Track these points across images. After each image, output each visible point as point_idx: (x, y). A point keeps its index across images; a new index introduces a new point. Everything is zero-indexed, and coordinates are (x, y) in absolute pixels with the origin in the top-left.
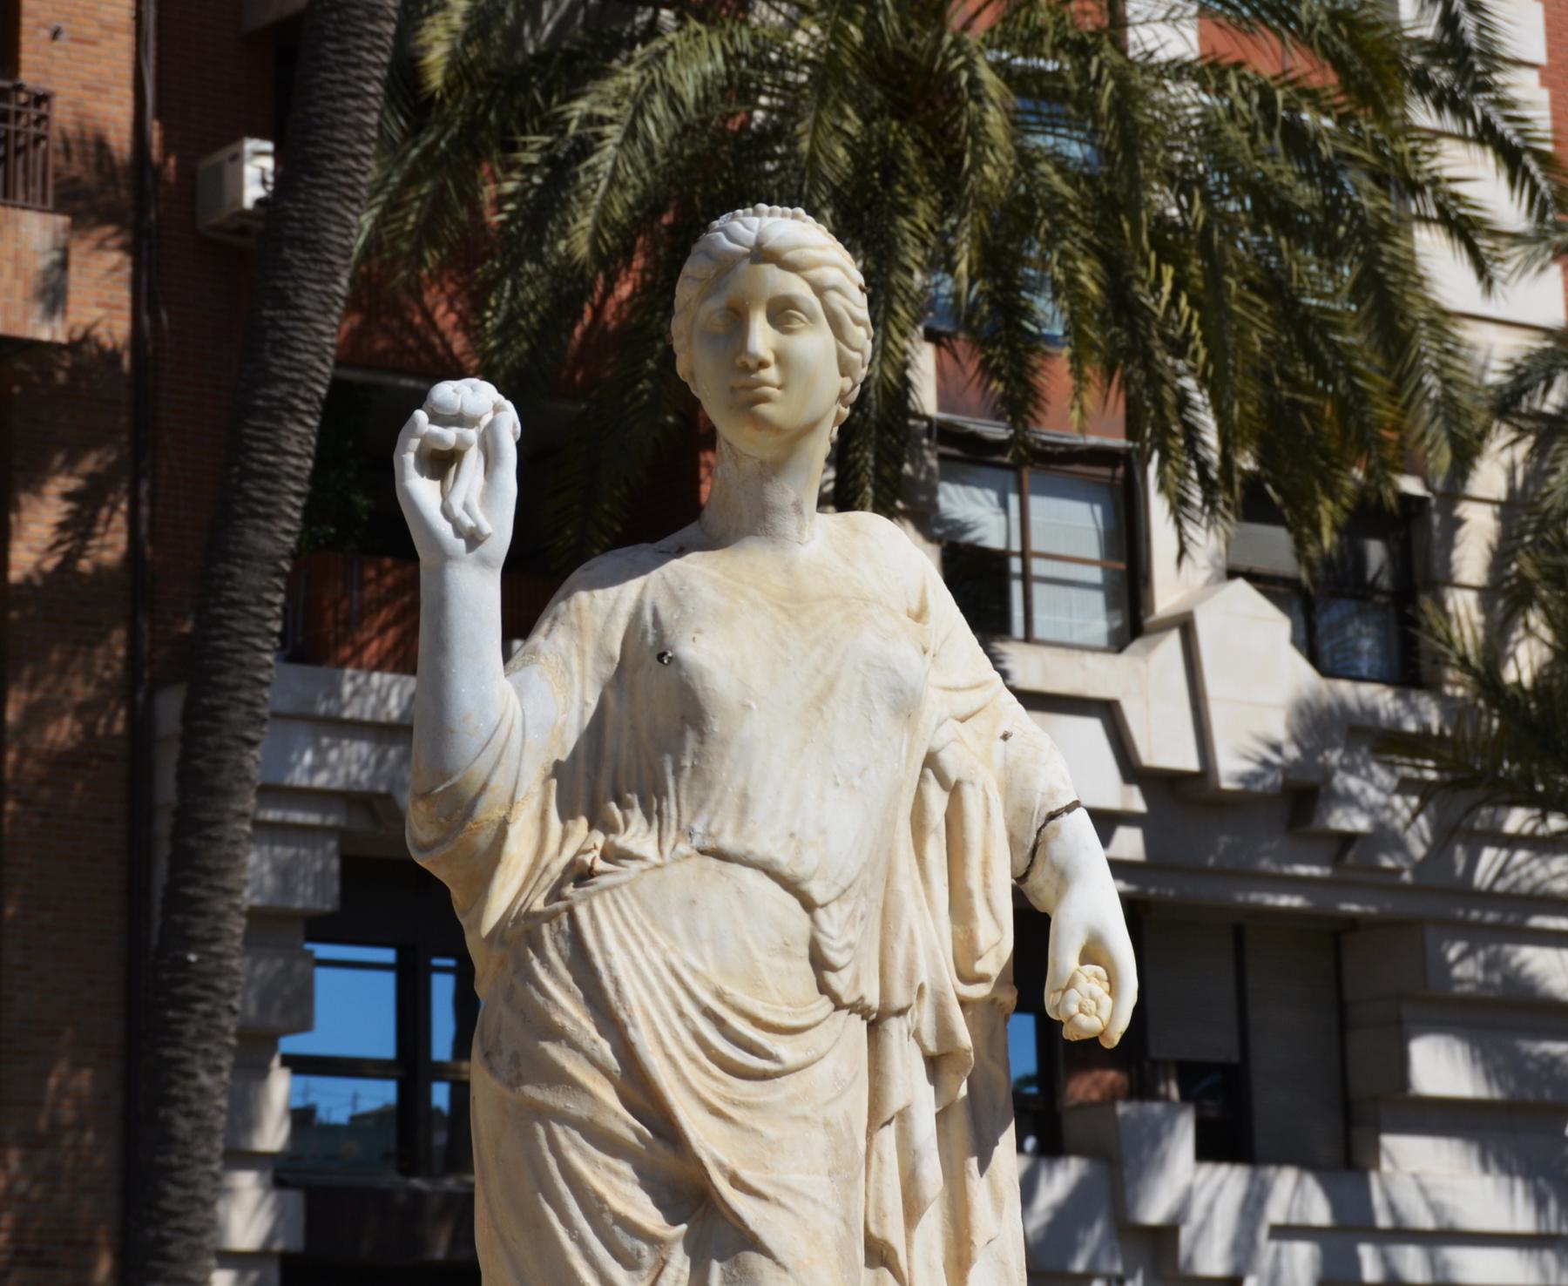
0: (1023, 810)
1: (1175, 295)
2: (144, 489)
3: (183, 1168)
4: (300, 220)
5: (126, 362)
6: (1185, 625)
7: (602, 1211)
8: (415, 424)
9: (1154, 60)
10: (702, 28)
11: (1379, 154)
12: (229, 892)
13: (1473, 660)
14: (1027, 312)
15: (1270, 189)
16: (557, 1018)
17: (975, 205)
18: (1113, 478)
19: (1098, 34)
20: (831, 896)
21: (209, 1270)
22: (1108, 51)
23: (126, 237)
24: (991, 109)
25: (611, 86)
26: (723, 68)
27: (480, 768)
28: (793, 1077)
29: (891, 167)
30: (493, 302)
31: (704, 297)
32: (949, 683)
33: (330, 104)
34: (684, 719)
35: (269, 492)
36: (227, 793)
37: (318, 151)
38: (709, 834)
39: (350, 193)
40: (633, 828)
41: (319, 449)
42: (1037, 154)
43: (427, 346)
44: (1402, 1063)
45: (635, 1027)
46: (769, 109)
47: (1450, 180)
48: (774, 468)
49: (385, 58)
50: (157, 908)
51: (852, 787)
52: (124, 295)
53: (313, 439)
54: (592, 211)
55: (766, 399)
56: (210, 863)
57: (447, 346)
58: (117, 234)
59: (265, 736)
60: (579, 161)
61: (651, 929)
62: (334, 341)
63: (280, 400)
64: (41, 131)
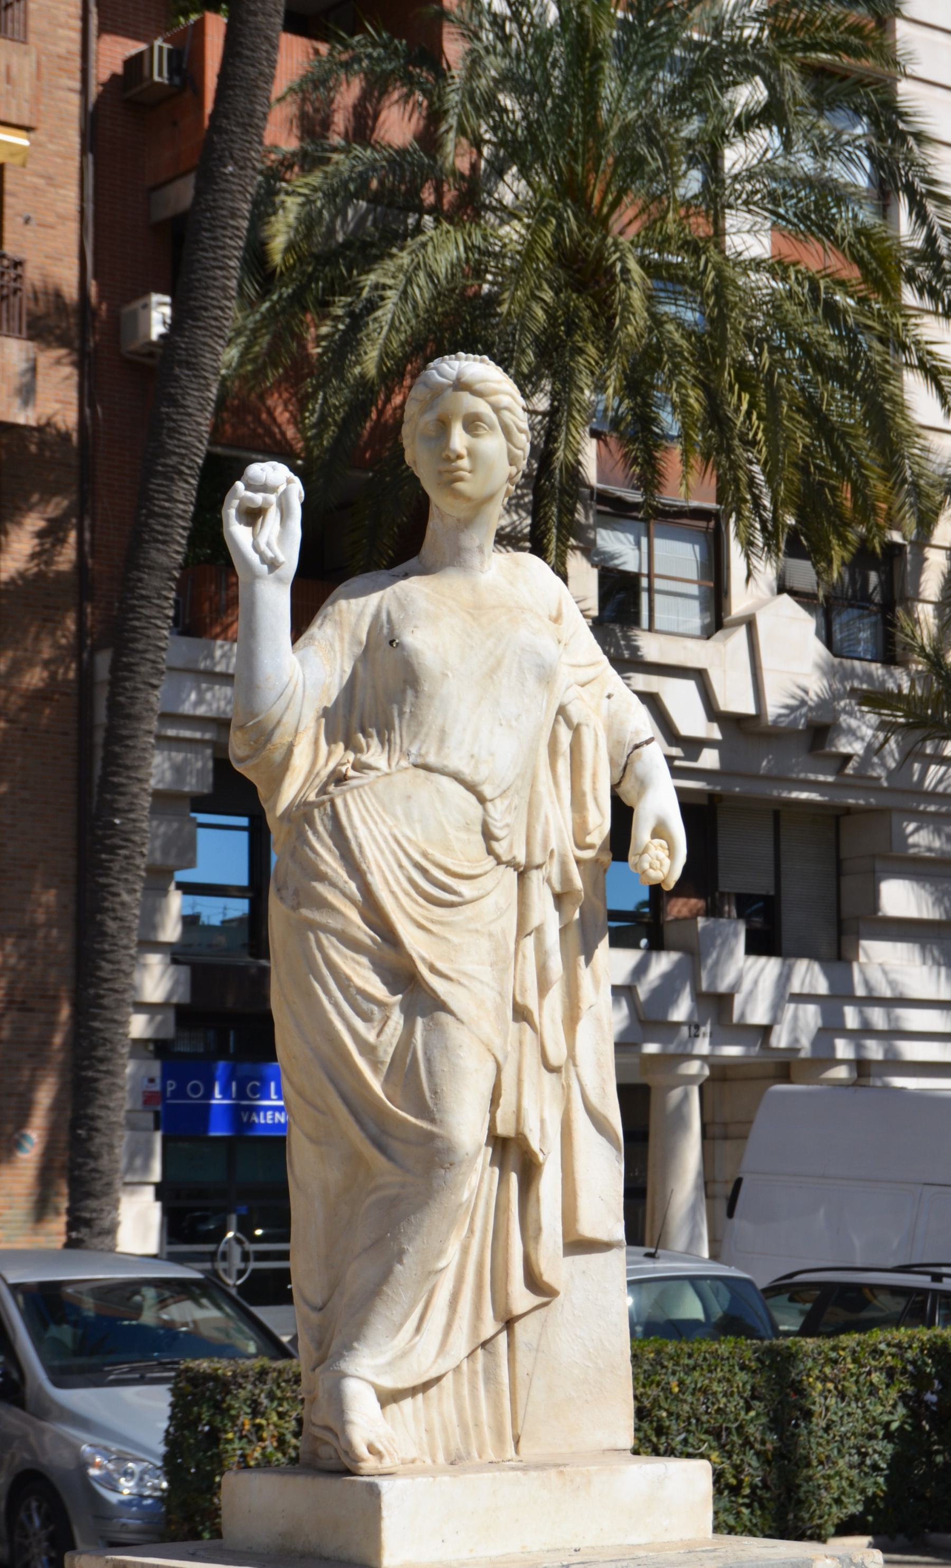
0: (619, 742)
1: (748, 414)
2: (87, 523)
3: (112, 951)
4: (186, 350)
5: (75, 437)
6: (750, 623)
7: (349, 986)
8: (236, 491)
9: (742, 258)
10: (451, 228)
11: (885, 325)
12: (140, 780)
13: (928, 649)
14: (655, 421)
15: (811, 344)
16: (323, 868)
17: (621, 351)
18: (707, 528)
19: (707, 239)
20: (496, 794)
21: (129, 1014)
22: (713, 252)
23: (74, 357)
24: (634, 288)
25: (390, 265)
26: (463, 255)
27: (276, 711)
28: (470, 906)
29: (570, 327)
30: (310, 407)
31: (423, 412)
32: (574, 662)
33: (206, 273)
34: (406, 682)
35: (165, 526)
36: (138, 718)
37: (197, 304)
38: (420, 755)
39: (218, 332)
40: (372, 750)
41: (198, 499)
42: (665, 318)
43: (272, 435)
44: (875, 895)
45: (371, 873)
46: (493, 284)
47: (927, 343)
48: (466, 524)
49: (241, 243)
50: (96, 789)
51: (511, 727)
52: (73, 396)
53: (194, 493)
54: (378, 346)
55: (461, 479)
56: (128, 762)
57: (283, 434)
58: (69, 355)
59: (165, 684)
60: (369, 314)
61: (382, 813)
62: (208, 429)
63: (173, 467)
64: (18, 285)
